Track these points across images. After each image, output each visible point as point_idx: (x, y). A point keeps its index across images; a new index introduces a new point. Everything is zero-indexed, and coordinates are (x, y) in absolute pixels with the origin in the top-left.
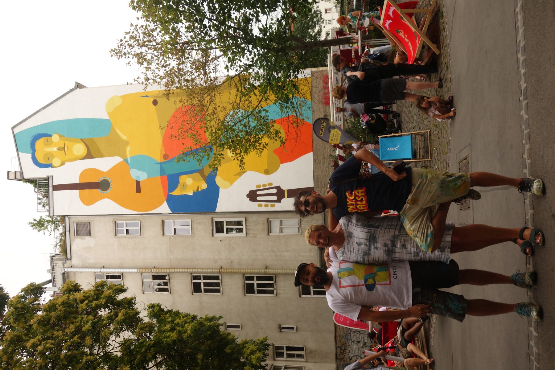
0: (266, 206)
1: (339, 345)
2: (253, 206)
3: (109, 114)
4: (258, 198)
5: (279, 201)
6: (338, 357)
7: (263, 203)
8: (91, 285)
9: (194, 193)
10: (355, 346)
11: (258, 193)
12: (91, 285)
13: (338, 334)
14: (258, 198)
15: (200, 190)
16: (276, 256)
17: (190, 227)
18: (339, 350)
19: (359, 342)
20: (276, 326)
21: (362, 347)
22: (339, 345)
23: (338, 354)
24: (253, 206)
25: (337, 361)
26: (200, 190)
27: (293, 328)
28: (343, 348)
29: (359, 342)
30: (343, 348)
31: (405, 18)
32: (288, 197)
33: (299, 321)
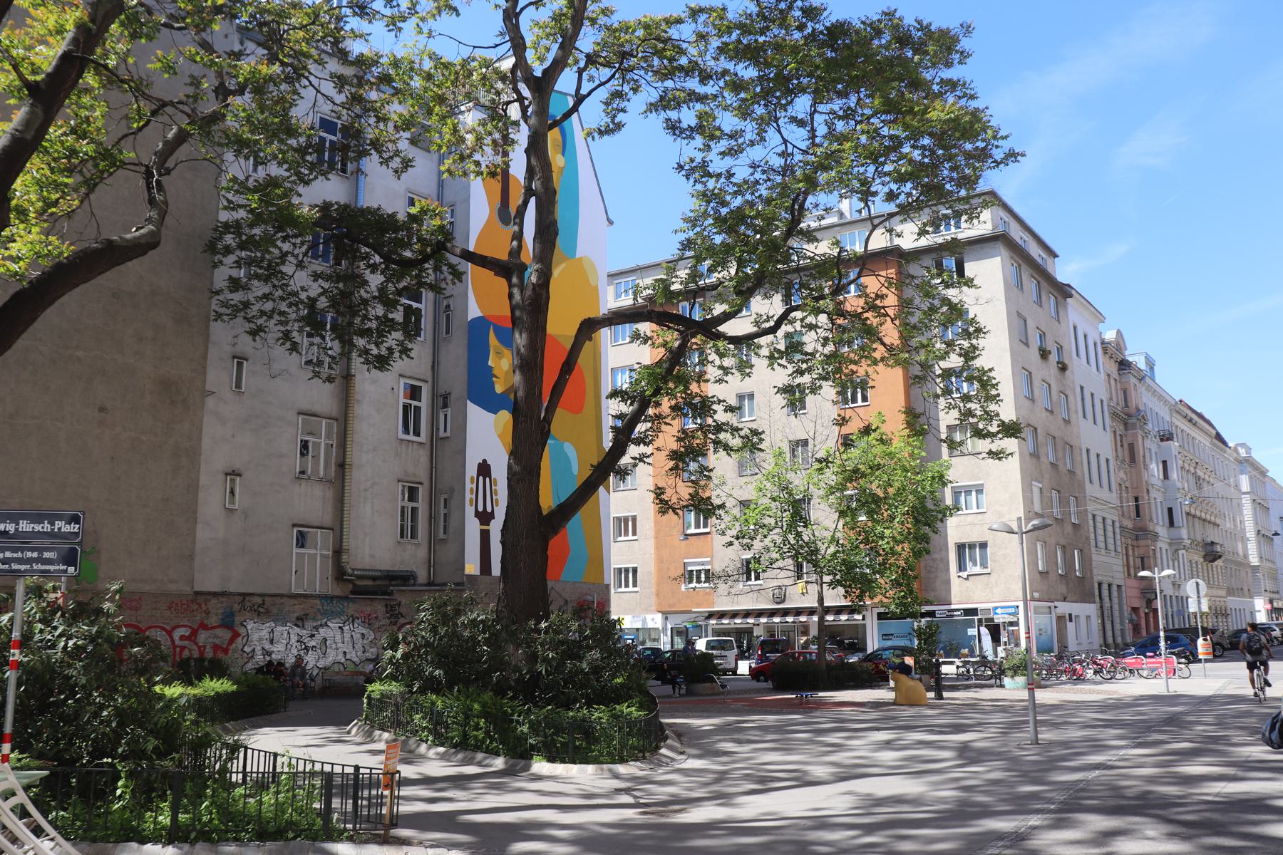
0: (472, 489)
1: (268, 600)
2: (471, 470)
3: (580, 259)
4: (481, 478)
5: (477, 514)
6: (247, 598)
7: (474, 486)
8: (248, 52)
9: (491, 368)
10: (265, 633)
11: (488, 479)
12: (248, 52)
13: (285, 600)
14: (481, 478)
15: (494, 379)
16: (366, 490)
17: (975, 511)
18: (259, 600)
19: (272, 642)
20: (237, 466)
21: (263, 649)
22: (268, 600)
23: (252, 598)
24: (471, 470)
25: (240, 594)
26: (494, 379)
27: (232, 502)
28: (261, 610)
29: (272, 642)
30: (261, 610)
31: (668, 718)
32: (481, 530)
33: (246, 517)
